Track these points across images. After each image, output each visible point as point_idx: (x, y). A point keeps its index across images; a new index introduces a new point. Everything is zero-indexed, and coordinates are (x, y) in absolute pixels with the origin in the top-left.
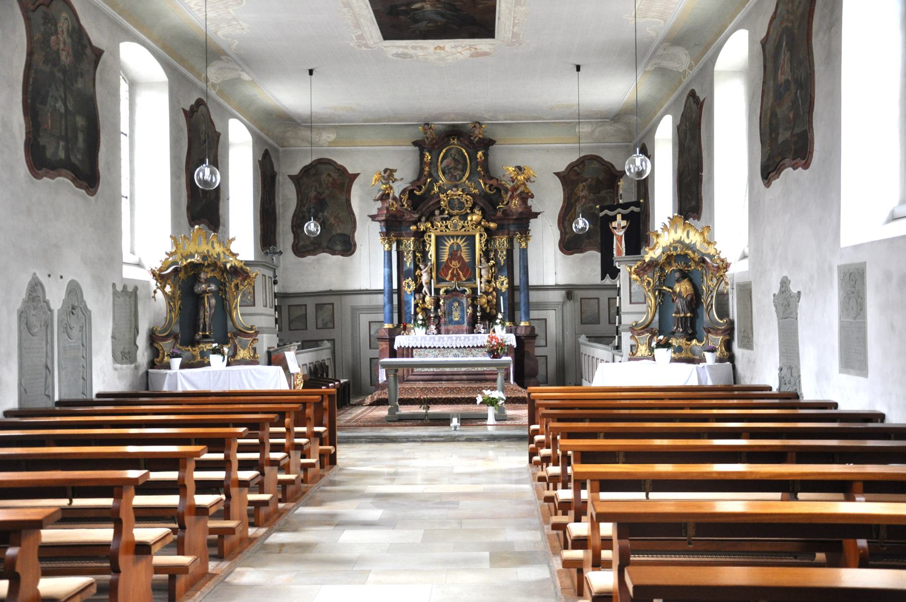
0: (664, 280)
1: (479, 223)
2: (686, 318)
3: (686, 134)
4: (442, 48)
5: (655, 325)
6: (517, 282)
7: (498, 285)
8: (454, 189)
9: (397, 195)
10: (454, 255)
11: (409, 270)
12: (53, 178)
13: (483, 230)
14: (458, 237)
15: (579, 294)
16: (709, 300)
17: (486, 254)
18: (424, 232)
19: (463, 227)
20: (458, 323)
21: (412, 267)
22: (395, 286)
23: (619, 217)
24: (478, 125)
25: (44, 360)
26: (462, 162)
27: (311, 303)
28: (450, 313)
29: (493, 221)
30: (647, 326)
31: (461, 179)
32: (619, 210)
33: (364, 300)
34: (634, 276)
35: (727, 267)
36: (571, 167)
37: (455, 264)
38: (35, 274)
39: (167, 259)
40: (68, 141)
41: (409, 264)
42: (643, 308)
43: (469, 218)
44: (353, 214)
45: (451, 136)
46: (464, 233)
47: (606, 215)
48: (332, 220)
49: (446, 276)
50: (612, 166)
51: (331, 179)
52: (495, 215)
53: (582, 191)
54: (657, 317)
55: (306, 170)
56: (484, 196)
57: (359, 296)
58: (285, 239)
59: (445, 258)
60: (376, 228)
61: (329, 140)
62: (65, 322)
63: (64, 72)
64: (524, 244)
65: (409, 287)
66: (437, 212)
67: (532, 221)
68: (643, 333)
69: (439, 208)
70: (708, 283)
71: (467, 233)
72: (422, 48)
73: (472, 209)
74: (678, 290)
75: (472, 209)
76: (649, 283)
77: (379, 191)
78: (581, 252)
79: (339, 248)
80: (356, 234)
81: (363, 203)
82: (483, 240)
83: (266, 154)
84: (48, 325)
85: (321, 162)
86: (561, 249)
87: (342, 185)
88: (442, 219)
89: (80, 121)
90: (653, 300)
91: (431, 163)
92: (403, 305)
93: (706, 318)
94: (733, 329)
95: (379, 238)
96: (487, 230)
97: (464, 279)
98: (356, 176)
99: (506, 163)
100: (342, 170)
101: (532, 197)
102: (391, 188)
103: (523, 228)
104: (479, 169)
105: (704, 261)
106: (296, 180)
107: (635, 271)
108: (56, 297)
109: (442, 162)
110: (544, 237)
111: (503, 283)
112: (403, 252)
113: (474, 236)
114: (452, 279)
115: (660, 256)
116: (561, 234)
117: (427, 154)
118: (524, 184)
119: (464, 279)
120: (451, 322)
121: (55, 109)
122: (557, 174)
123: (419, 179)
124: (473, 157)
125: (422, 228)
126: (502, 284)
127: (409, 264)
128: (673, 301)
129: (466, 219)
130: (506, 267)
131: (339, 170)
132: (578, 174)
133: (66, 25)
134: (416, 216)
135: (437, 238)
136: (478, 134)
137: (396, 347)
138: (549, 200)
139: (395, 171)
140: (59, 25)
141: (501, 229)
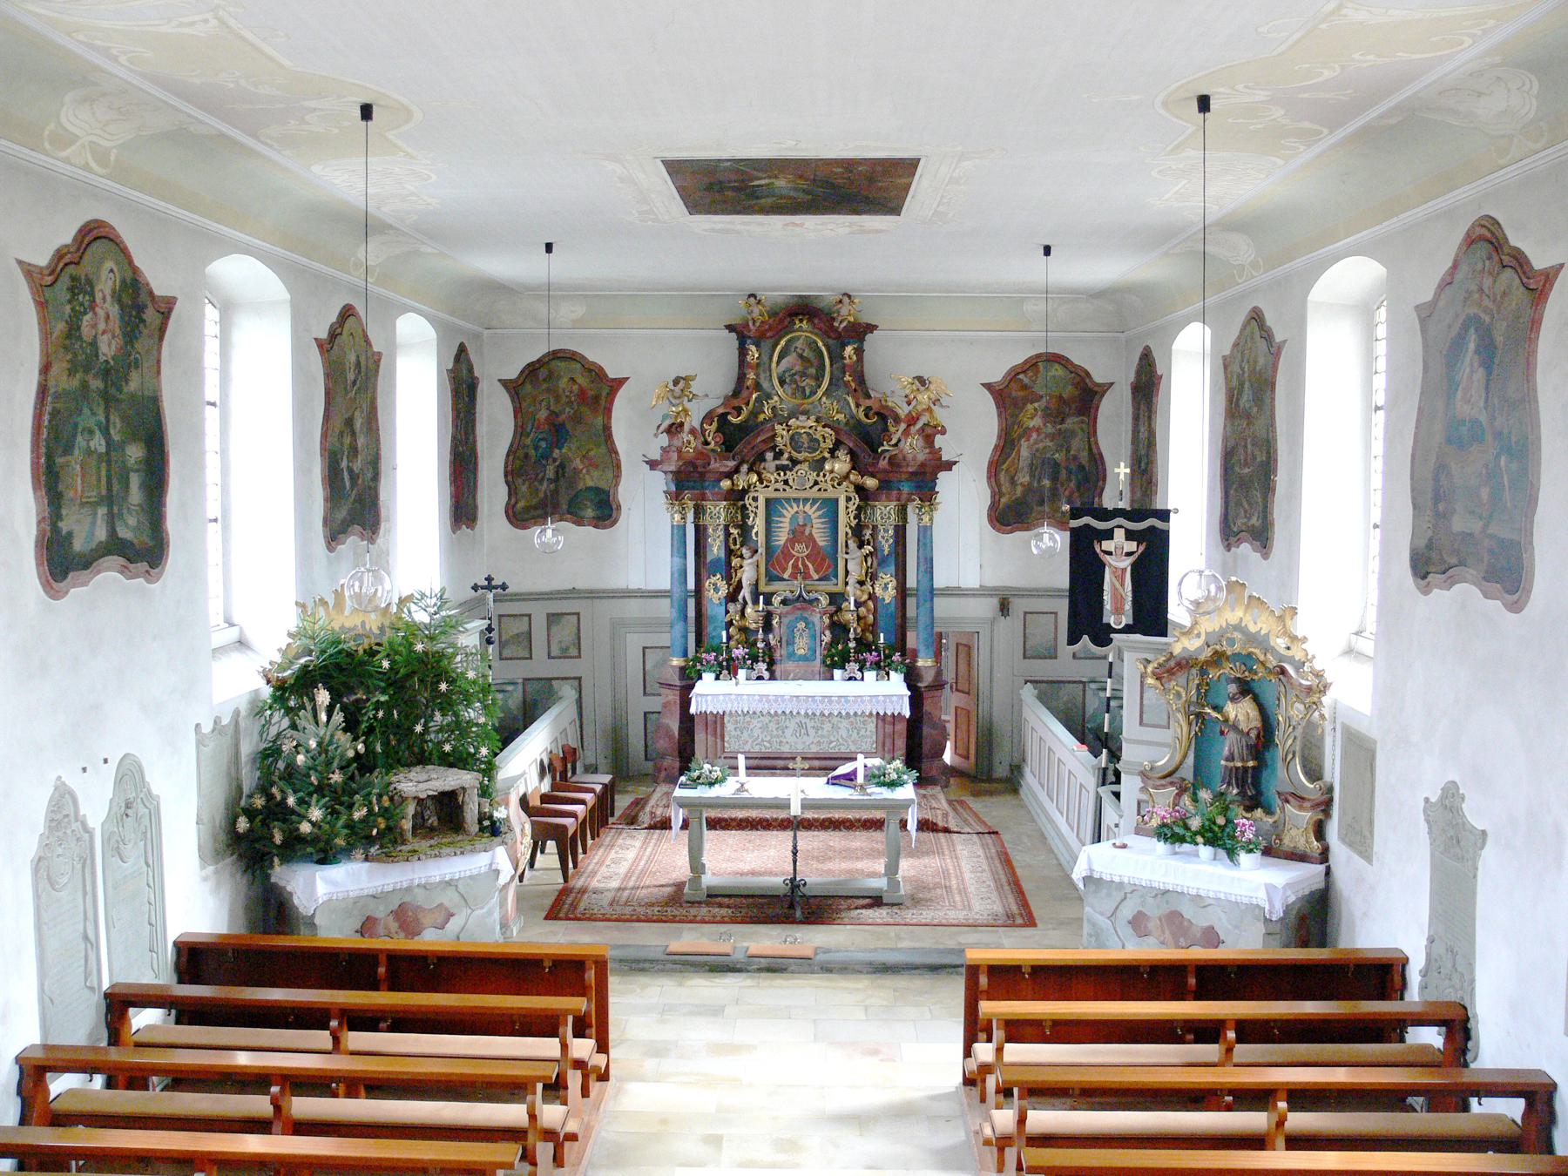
0: (1205, 694)
1: (846, 477)
2: (1245, 769)
3: (1242, 385)
4: (802, 225)
5: (1187, 772)
6: (911, 582)
7: (878, 591)
8: (802, 418)
9: (697, 425)
10: (798, 534)
11: (718, 560)
12: (85, 584)
13: (852, 488)
14: (806, 500)
15: (1019, 606)
16: (1284, 740)
17: (857, 531)
18: (745, 492)
19: (816, 483)
20: (805, 658)
21: (722, 555)
22: (691, 585)
23: (1119, 534)
24: (846, 300)
25: (81, 927)
26: (815, 362)
27: (539, 612)
28: (791, 642)
29: (873, 475)
30: (1170, 775)
31: (813, 393)
32: (1120, 521)
33: (634, 608)
34: (1150, 681)
35: (1323, 689)
36: (1014, 375)
37: (800, 550)
38: (59, 778)
39: (289, 645)
40: (110, 483)
41: (716, 549)
42: (1166, 736)
43: (827, 467)
44: (616, 453)
45: (797, 314)
46: (818, 495)
47: (1087, 526)
48: (578, 463)
49: (784, 570)
50: (1088, 374)
51: (576, 387)
52: (874, 465)
53: (1033, 418)
54: (1190, 760)
55: (532, 370)
56: (857, 428)
57: (626, 600)
58: (492, 491)
59: (782, 538)
60: (659, 482)
61: (574, 316)
62: (117, 837)
63: (106, 373)
64: (926, 518)
65: (716, 590)
66: (769, 456)
67: (942, 475)
68: (1164, 786)
69: (773, 448)
70: (1289, 712)
71: (825, 495)
72: (760, 224)
73: (832, 452)
74: (1232, 716)
75: (832, 452)
76: (1178, 695)
77: (665, 417)
78: (1027, 529)
79: (590, 513)
80: (620, 489)
81: (634, 430)
82: (853, 508)
83: (462, 349)
84: (87, 861)
85: (555, 355)
86: (991, 521)
87: (597, 398)
88: (778, 468)
89: (135, 452)
90: (1185, 729)
91: (758, 365)
92: (705, 622)
93: (1281, 772)
94: (1331, 800)
95: (662, 500)
96: (860, 489)
97: (816, 576)
98: (620, 382)
99: (893, 365)
100: (596, 373)
101: (943, 432)
102: (685, 411)
103: (927, 493)
104: (847, 378)
105: (1283, 672)
106: (513, 388)
107: (1154, 673)
108: (95, 807)
109: (778, 363)
110: (963, 498)
111: (886, 589)
112: (705, 528)
113: (836, 501)
114: (793, 576)
115: (1200, 649)
116: (993, 497)
117: (753, 348)
118: (929, 410)
119: (816, 576)
120: (791, 655)
121: (89, 452)
122: (988, 386)
123: (736, 394)
124: (836, 357)
125: (741, 484)
126: (886, 588)
127: (716, 549)
128: (1222, 733)
129: (822, 469)
130: (892, 560)
131: (590, 371)
132: (1025, 387)
133: (110, 283)
134: (732, 464)
135: (768, 501)
136: (846, 315)
137: (693, 710)
138: (971, 434)
139: (693, 378)
140: (97, 289)
141: (885, 485)
